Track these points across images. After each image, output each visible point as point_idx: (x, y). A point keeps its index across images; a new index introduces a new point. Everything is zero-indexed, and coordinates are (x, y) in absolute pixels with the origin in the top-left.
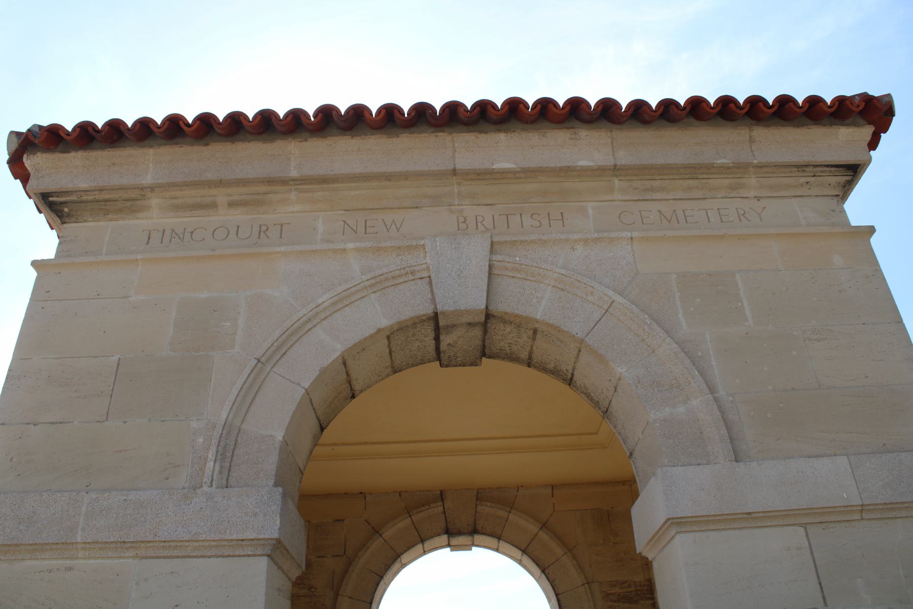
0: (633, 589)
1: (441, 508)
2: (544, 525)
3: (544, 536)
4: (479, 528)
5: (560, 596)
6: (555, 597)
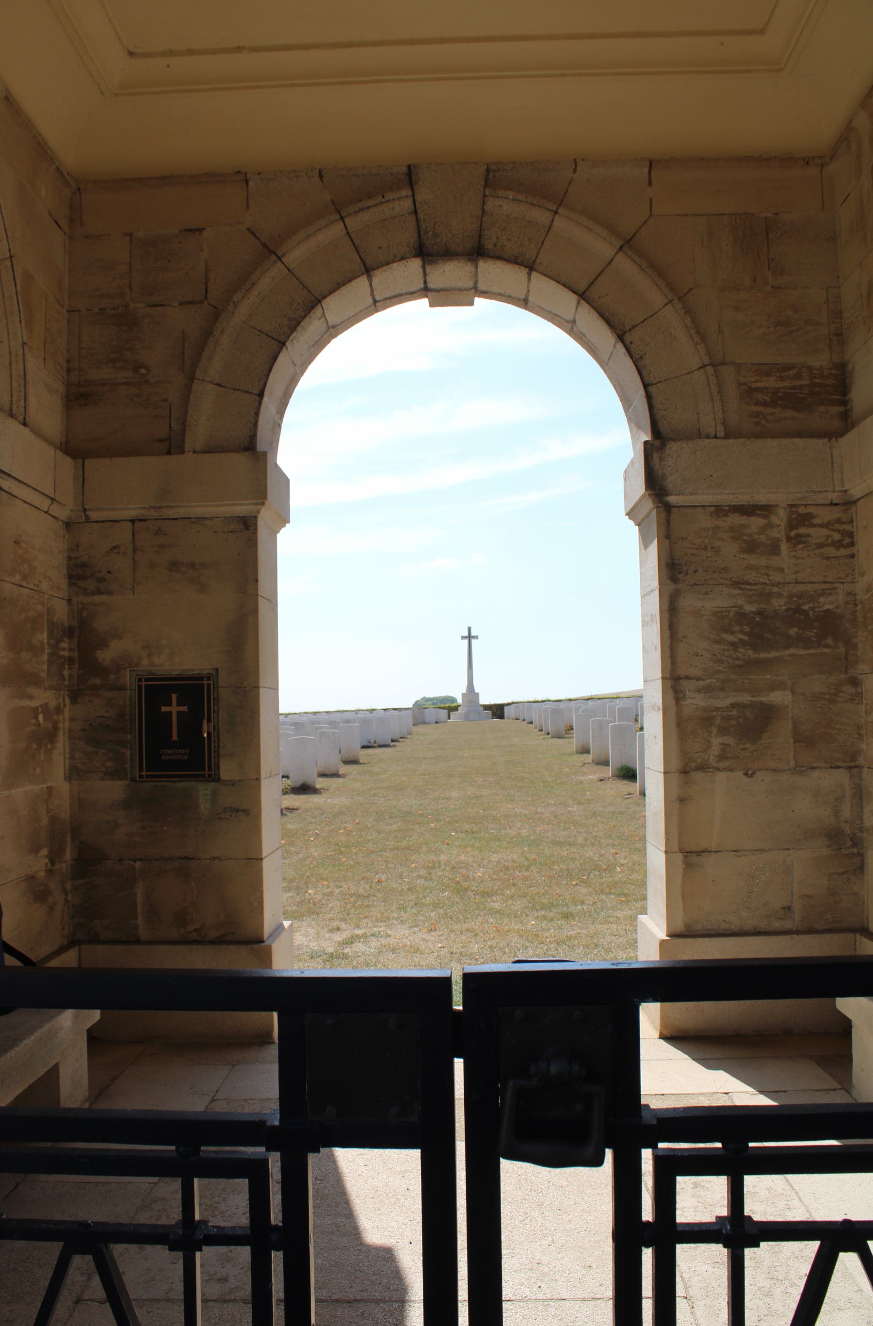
0: (805, 382)
1: (408, 203)
2: (628, 242)
3: (625, 265)
4: (488, 245)
5: (651, 389)
6: (641, 392)
